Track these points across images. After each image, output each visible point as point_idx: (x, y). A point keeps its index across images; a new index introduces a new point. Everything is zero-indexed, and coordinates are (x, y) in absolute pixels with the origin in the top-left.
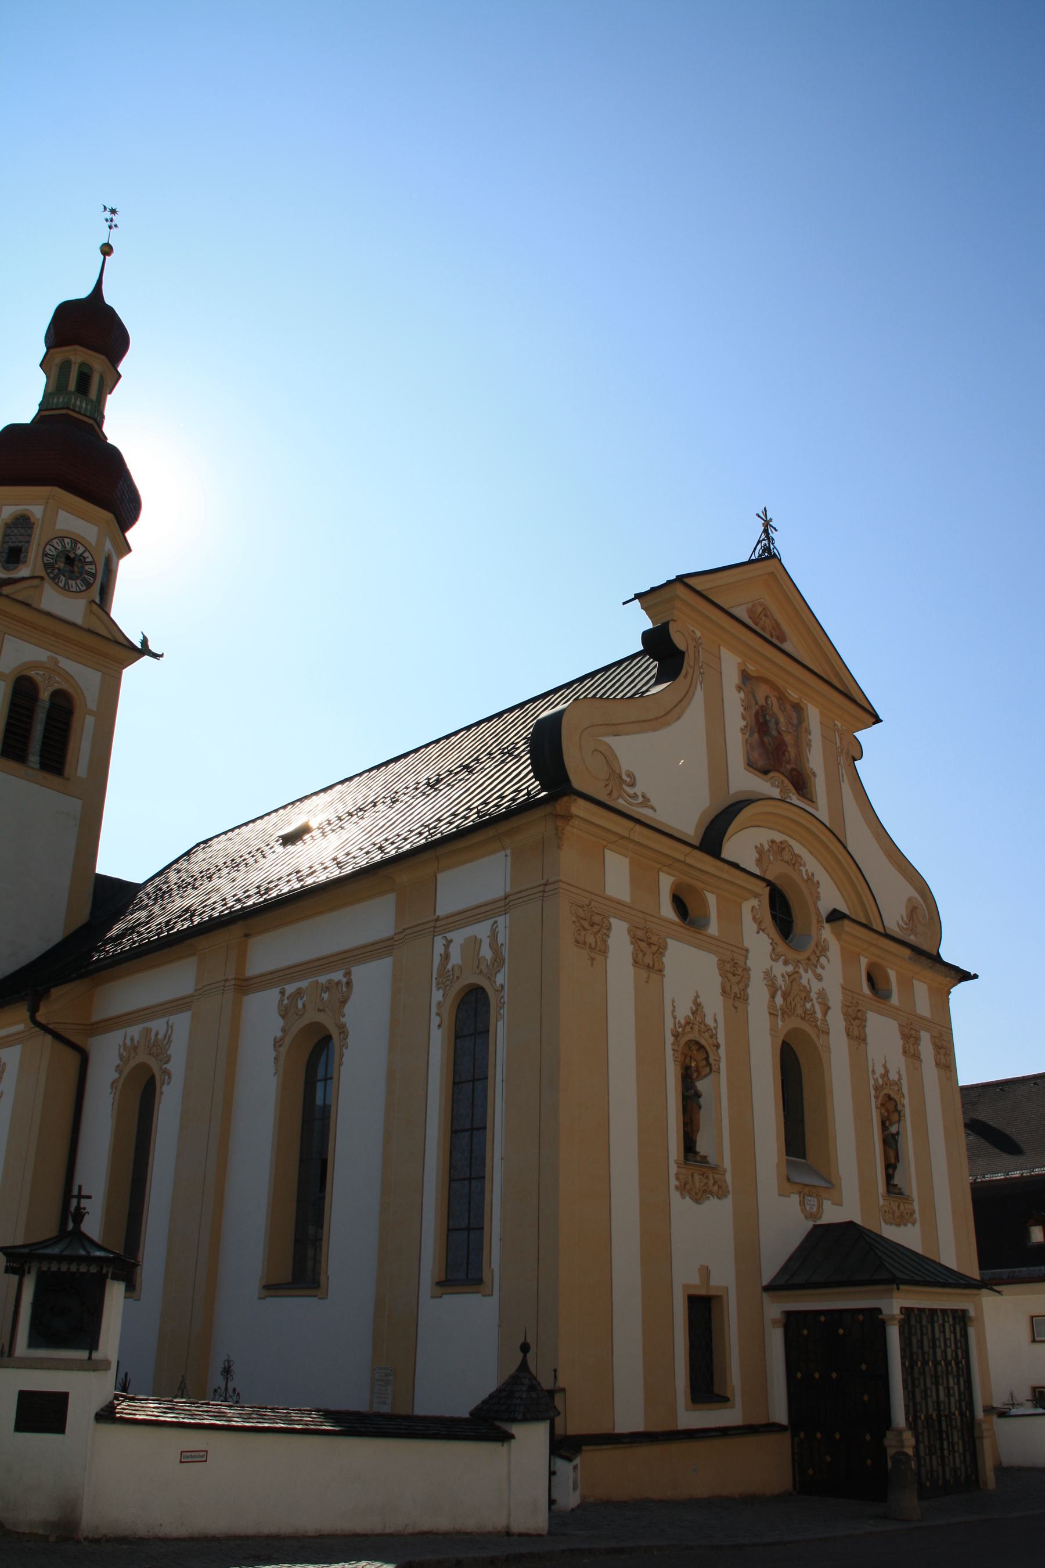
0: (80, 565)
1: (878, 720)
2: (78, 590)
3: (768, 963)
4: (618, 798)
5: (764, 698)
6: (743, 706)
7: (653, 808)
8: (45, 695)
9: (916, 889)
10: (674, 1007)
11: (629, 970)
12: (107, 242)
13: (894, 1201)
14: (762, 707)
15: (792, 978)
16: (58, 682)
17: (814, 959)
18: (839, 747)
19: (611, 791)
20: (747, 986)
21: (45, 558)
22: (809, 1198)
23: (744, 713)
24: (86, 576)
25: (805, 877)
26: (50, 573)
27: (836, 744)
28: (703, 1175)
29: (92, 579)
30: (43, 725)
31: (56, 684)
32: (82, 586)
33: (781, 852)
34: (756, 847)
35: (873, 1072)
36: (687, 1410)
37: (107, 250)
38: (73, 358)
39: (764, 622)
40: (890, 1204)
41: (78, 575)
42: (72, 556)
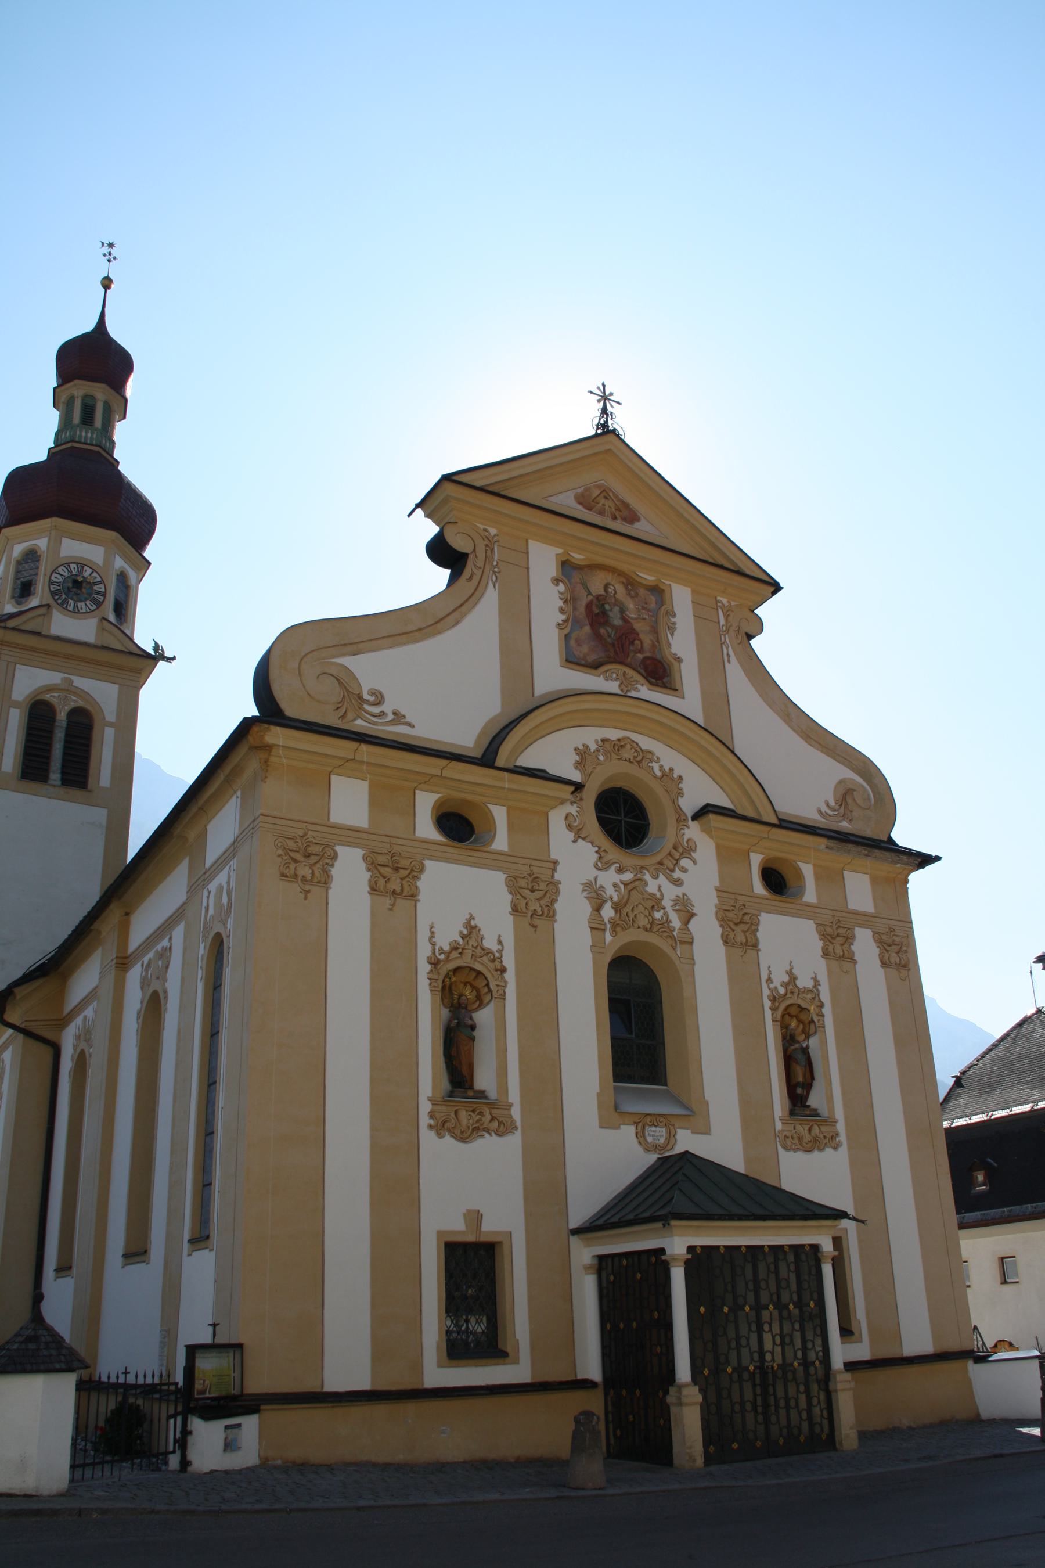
0: (88, 586)
1: (776, 588)
2: (88, 610)
3: (591, 873)
4: (355, 720)
5: (602, 586)
6: (562, 599)
7: (409, 724)
8: (62, 716)
9: (853, 770)
10: (433, 933)
11: (364, 899)
12: (106, 275)
13: (801, 1124)
14: (598, 597)
15: (630, 887)
16: (74, 701)
17: (669, 863)
18: (723, 626)
19: (345, 712)
20: (554, 901)
21: (52, 586)
22: (653, 1128)
23: (564, 606)
24: (95, 596)
25: (659, 774)
26: (57, 599)
27: (719, 623)
28: (473, 1111)
29: (102, 598)
30: (62, 743)
31: (72, 703)
32: (92, 606)
33: (618, 750)
34: (576, 749)
35: (769, 980)
36: (440, 1365)
37: (107, 283)
38: (76, 393)
39: (604, 505)
40: (794, 1128)
41: (86, 596)
42: (80, 579)
